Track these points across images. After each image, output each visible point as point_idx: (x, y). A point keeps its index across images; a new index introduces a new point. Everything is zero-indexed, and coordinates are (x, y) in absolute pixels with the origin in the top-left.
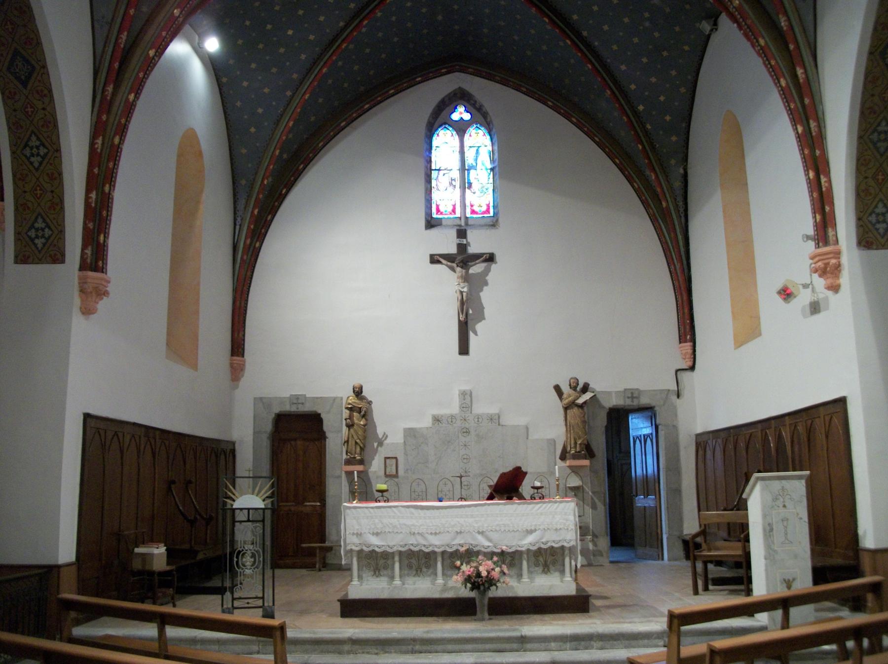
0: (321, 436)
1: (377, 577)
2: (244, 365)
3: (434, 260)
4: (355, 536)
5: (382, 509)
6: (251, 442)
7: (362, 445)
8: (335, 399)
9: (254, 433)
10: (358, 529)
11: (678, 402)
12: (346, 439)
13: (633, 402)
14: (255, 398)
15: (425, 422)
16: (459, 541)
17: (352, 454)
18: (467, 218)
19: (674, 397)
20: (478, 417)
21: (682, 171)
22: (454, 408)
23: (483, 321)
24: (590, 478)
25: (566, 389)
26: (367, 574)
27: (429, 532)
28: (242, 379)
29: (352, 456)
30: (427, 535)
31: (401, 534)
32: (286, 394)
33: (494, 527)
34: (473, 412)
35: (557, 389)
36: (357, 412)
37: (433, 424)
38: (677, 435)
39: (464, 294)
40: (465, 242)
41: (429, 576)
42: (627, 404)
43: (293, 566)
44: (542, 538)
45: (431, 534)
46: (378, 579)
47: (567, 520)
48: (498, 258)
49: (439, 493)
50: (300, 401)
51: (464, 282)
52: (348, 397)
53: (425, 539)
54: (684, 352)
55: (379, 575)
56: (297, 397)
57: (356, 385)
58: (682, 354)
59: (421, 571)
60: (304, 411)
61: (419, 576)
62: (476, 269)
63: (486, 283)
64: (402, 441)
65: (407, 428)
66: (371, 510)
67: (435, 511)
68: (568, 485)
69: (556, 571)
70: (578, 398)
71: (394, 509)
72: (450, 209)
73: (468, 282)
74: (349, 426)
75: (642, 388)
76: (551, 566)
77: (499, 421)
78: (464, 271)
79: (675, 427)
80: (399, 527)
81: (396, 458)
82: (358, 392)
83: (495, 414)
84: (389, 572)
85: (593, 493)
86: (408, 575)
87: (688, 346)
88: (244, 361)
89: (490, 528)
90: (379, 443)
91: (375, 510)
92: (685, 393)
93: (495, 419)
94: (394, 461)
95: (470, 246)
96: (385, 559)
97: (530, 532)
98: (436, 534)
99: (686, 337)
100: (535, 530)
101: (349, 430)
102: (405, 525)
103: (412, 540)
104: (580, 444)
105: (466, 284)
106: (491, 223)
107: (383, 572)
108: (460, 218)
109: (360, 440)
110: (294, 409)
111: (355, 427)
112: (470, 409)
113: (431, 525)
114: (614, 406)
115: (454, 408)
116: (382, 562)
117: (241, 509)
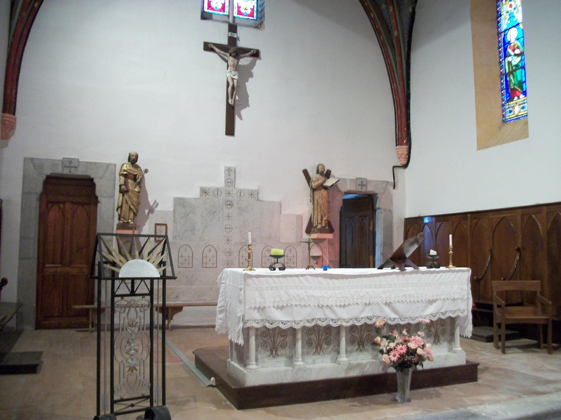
0: (95, 201)
1: (274, 357)
2: (15, 123)
3: (208, 47)
4: (256, 311)
5: (288, 278)
6: (20, 201)
7: (135, 211)
8: (108, 165)
9: (23, 193)
10: (260, 303)
11: (394, 192)
12: (120, 204)
13: (362, 188)
14: (25, 159)
15: (193, 194)
16: (367, 313)
17: (125, 219)
18: (234, 17)
19: (392, 188)
20: (240, 192)
21: (410, 9)
22: (220, 182)
23: (247, 108)
24: (328, 249)
25: (313, 174)
26: (264, 355)
27: (338, 304)
28: (12, 138)
29: (125, 221)
30: (335, 308)
31: (308, 307)
32: (59, 156)
33: (400, 298)
34: (235, 187)
35: (305, 172)
36: (132, 179)
37: (201, 195)
38: (392, 217)
39: (235, 81)
40: (236, 36)
41: (330, 353)
42: (358, 190)
43: (58, 327)
44: (441, 309)
45: (340, 306)
46: (275, 360)
47: (462, 290)
48: (262, 55)
49: (180, 258)
50: (73, 164)
51: (235, 70)
52: (123, 165)
53: (334, 312)
54: (400, 153)
55: (276, 355)
56: (70, 161)
57: (133, 153)
58: (398, 154)
59: (321, 349)
60: (77, 175)
61: (319, 354)
62: (245, 61)
63: (251, 75)
64: (172, 209)
65: (177, 198)
66: (276, 279)
67: (345, 280)
68: (311, 255)
69: (444, 341)
70: (325, 182)
71: (301, 278)
72: (220, 6)
73: (238, 71)
74: (123, 192)
75: (368, 179)
76: (440, 336)
77: (258, 197)
78: (236, 61)
79: (390, 211)
80: (306, 299)
81: (166, 225)
82: (133, 160)
83: (255, 190)
84: (287, 351)
85: (330, 261)
86: (308, 353)
87: (404, 148)
88: (15, 119)
89: (396, 299)
90: (149, 210)
91: (281, 279)
92: (399, 185)
93: (254, 194)
94: (164, 227)
95: (239, 41)
96: (284, 336)
97: (431, 302)
98: (345, 306)
99: (402, 141)
100: (436, 300)
101: (123, 195)
102: (313, 296)
103: (319, 314)
104: (325, 220)
105: (237, 73)
106: (254, 25)
107: (281, 352)
108: (228, 16)
109: (134, 206)
110: (66, 172)
111: (130, 193)
112: (233, 184)
113: (340, 296)
114: (348, 191)
115: (220, 182)
116: (279, 340)
117: (142, 279)
